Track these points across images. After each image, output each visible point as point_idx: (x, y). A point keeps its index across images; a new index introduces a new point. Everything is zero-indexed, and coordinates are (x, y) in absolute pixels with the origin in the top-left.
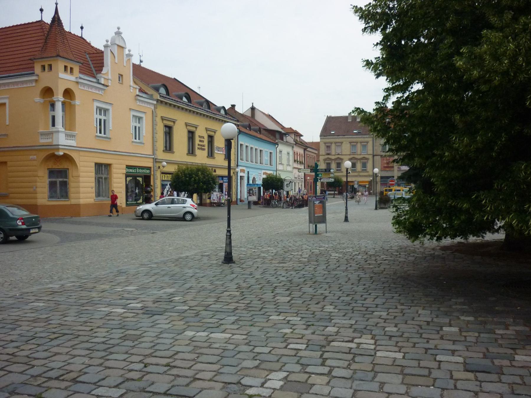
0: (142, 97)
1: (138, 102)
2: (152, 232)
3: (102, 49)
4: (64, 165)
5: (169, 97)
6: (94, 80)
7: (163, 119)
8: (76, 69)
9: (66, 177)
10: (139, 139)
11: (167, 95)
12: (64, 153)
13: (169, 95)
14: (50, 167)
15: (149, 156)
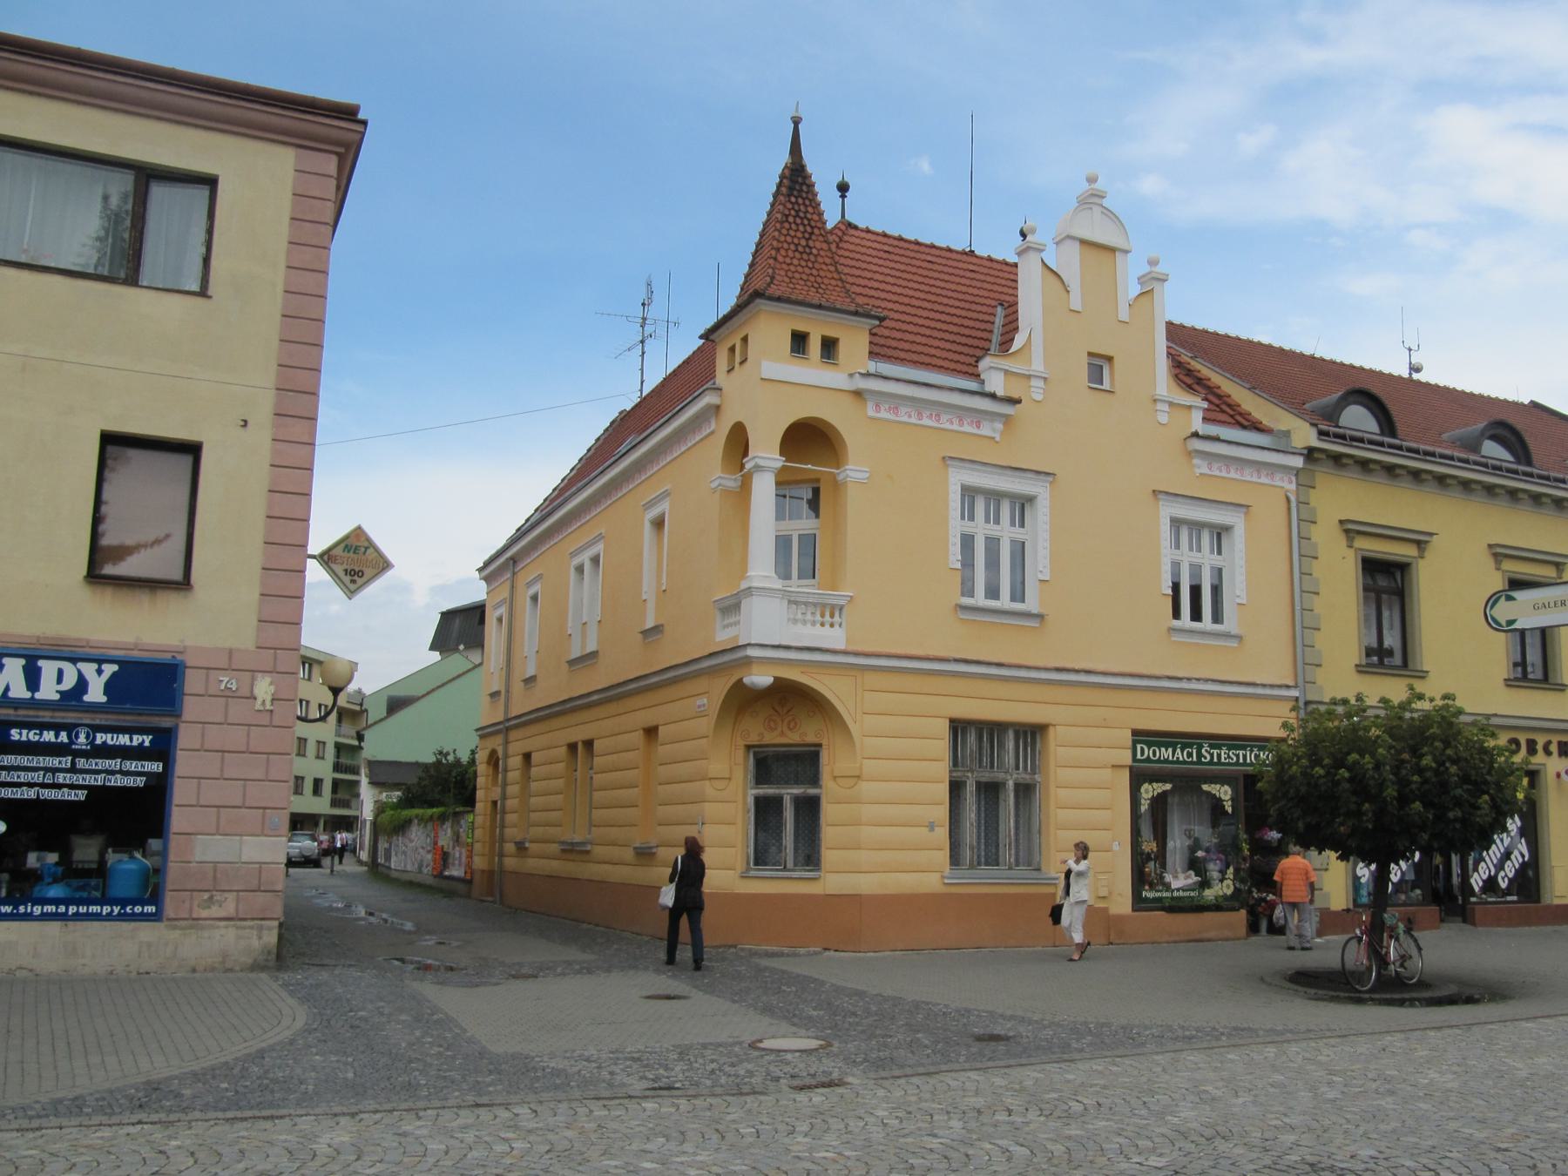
0: (1217, 439)
1: (1196, 461)
2: (470, 1099)
3: (1012, 259)
4: (804, 732)
5: (1528, 469)
6: (972, 385)
7: (1351, 530)
8: (855, 341)
9: (815, 780)
10: (1217, 617)
11: (1382, 433)
12: (776, 679)
13: (1393, 434)
14: (754, 739)
15: (1268, 691)
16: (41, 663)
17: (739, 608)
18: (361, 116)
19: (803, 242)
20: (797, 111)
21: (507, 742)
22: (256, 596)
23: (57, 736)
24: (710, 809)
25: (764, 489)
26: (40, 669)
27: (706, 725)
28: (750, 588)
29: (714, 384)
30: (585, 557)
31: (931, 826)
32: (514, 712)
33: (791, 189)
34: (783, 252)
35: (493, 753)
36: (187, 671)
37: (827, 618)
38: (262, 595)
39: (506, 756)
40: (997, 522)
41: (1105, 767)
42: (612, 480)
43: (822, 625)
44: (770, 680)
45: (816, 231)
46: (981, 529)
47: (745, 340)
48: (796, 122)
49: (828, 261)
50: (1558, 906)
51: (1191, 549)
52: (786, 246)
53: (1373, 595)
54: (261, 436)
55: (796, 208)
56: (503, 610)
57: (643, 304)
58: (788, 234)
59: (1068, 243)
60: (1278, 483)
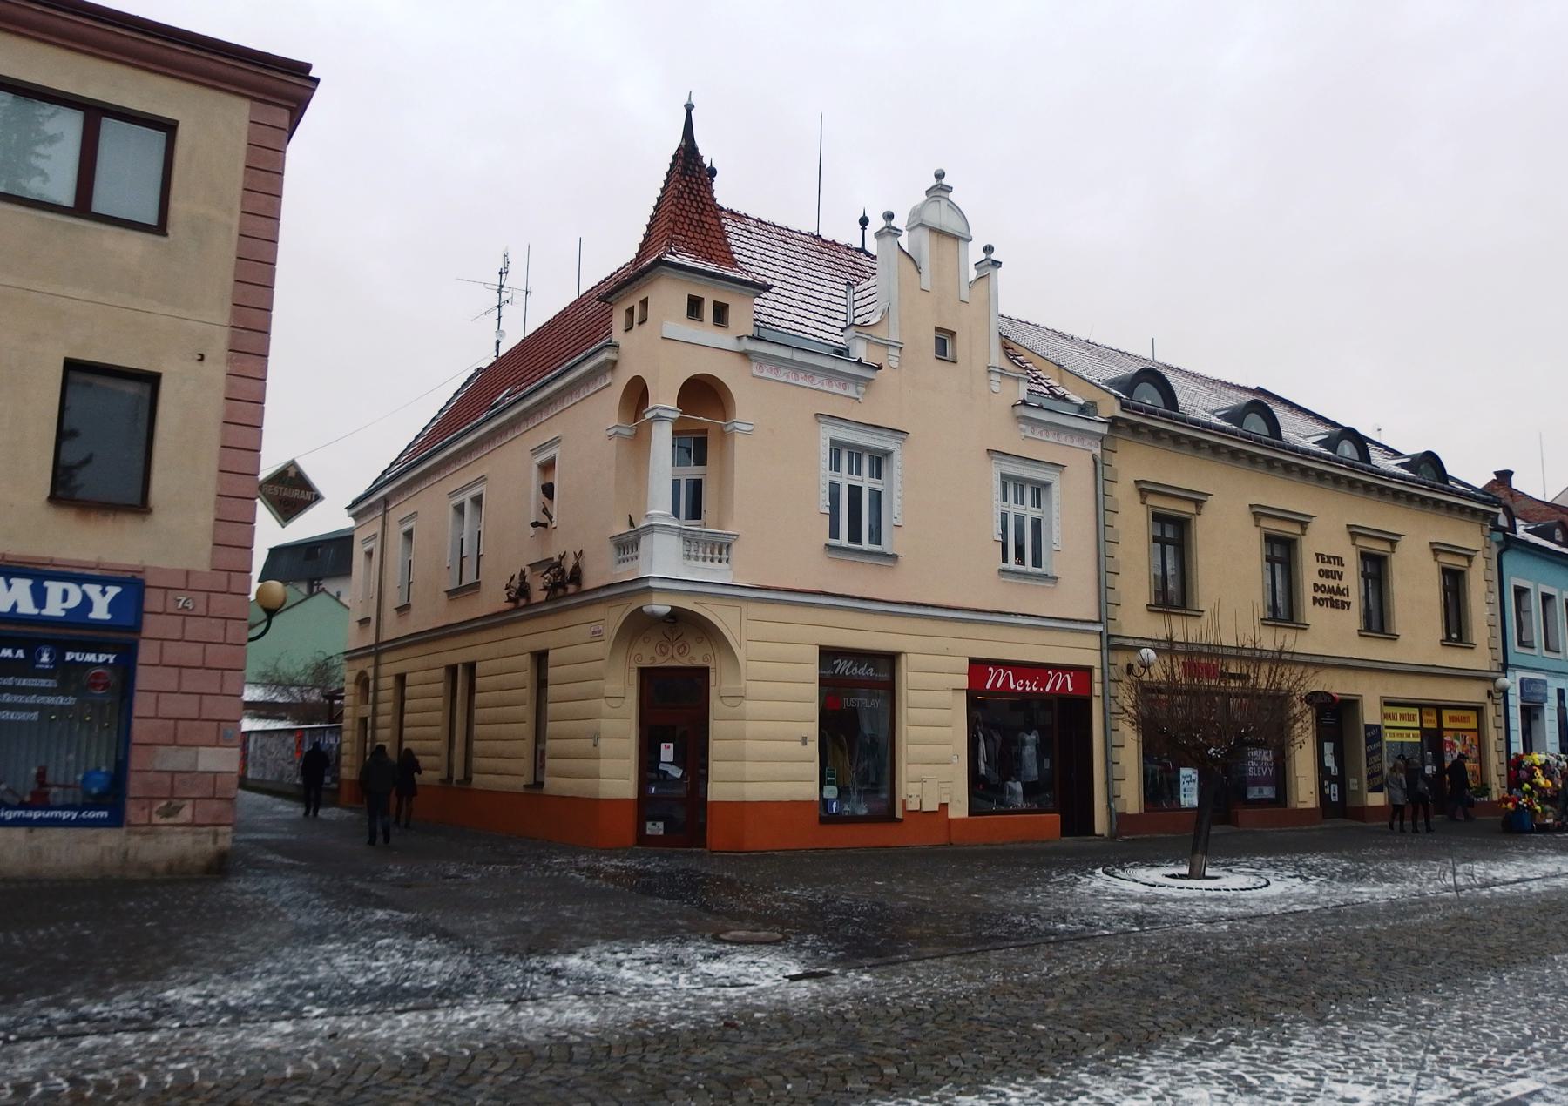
4: (694, 656)
7: (1144, 490)
16: (47, 584)
17: (637, 545)
18: (312, 74)
19: (696, 217)
20: (690, 99)
21: (377, 665)
22: (212, 520)
23: (14, 652)
24: (605, 725)
25: (662, 439)
26: (46, 589)
27: (602, 648)
28: (652, 525)
29: (611, 341)
30: (466, 497)
31: (804, 741)
32: (386, 637)
33: (685, 168)
34: (680, 225)
35: (362, 674)
36: (147, 590)
37: (717, 555)
38: (217, 520)
39: (377, 677)
40: (858, 473)
41: (947, 690)
42: (499, 427)
43: (720, 561)
44: (668, 609)
45: (707, 208)
46: (845, 479)
47: (644, 303)
48: (689, 108)
49: (718, 235)
50: (1302, 809)
51: (1016, 502)
52: (682, 219)
53: (1159, 545)
54: (216, 371)
55: (690, 185)
56: (375, 545)
57: (501, 273)
58: (684, 209)
59: (920, 230)
60: (1088, 447)
